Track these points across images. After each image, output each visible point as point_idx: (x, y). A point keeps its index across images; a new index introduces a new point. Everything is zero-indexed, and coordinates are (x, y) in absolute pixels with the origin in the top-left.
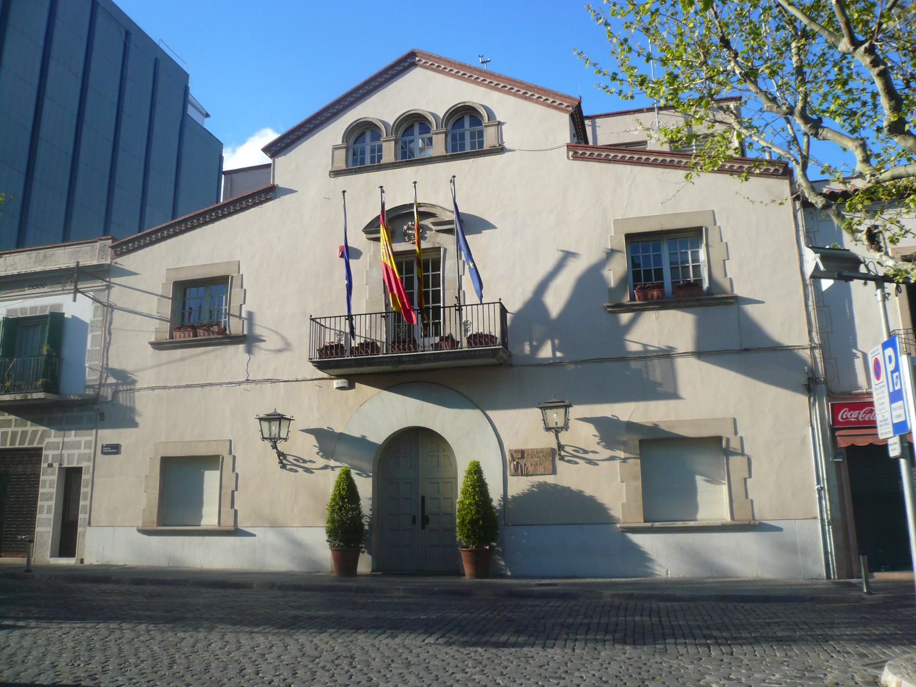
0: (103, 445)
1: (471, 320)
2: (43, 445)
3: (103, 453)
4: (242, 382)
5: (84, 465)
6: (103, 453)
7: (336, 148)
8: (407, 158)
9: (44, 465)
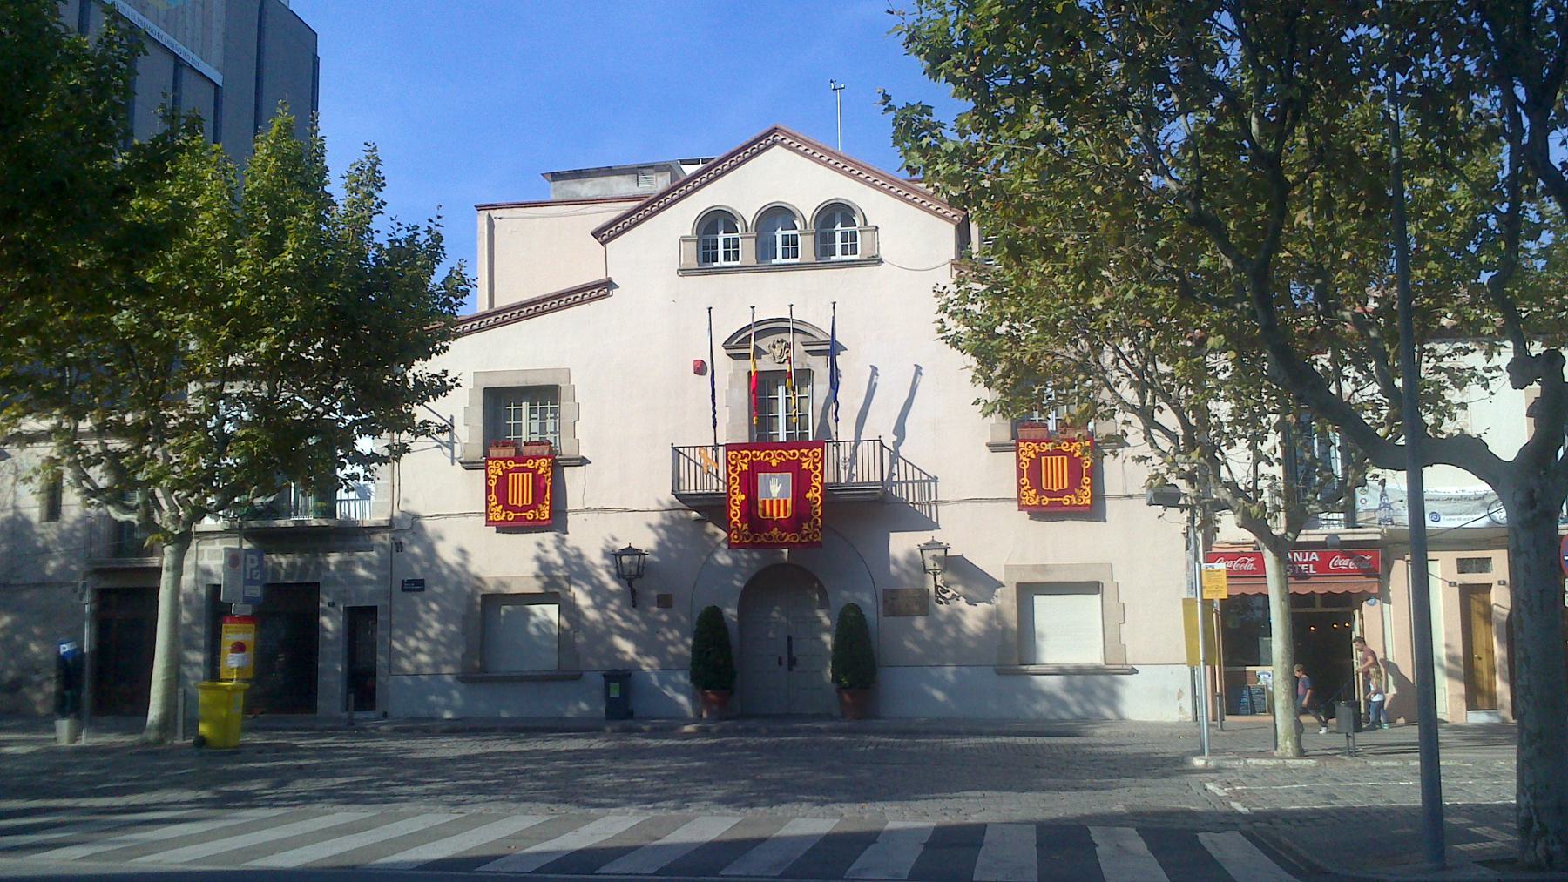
0: (403, 581)
2: (320, 580)
3: (403, 590)
4: (581, 511)
5: (379, 602)
7: (684, 240)
8: (765, 260)
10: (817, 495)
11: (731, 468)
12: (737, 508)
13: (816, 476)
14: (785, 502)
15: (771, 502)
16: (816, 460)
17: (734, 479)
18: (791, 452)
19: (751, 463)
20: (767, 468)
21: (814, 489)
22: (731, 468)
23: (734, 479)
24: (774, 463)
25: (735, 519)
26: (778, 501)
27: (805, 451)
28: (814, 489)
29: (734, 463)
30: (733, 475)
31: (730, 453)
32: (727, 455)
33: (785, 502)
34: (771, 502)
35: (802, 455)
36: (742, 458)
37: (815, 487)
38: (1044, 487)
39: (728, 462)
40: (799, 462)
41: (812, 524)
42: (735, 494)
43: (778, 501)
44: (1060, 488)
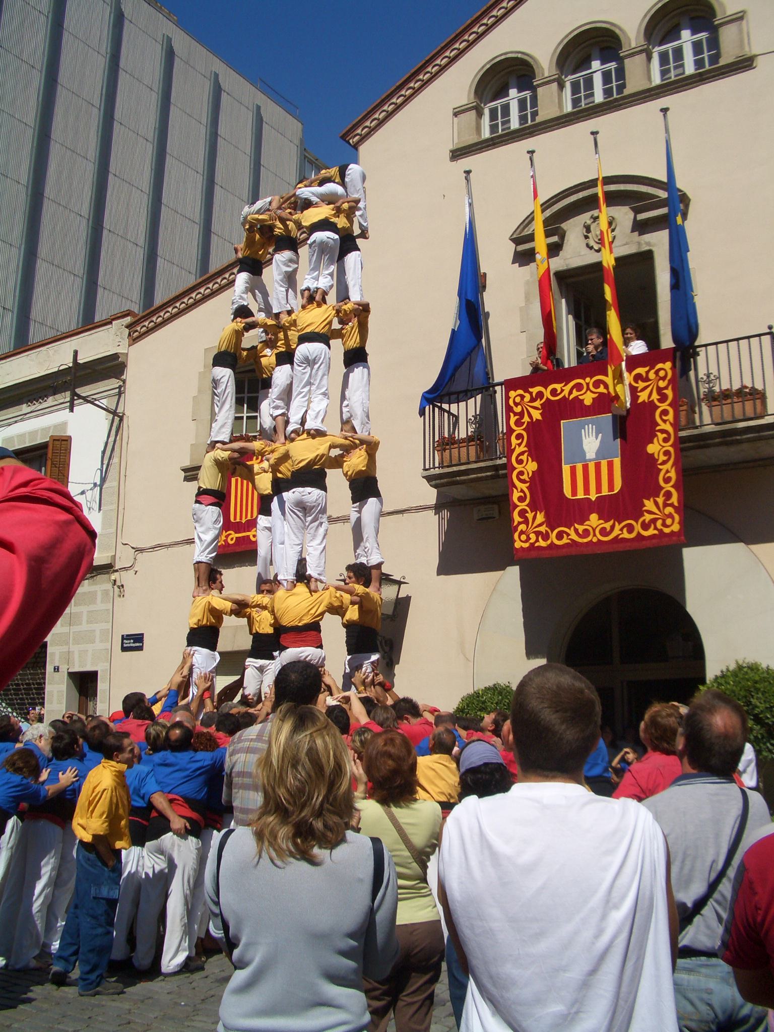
1: (716, 373)
5: (100, 667)
6: (124, 649)
9: (49, 668)
10: (519, 468)
11: (513, 419)
12: (524, 487)
13: (665, 412)
14: (610, 465)
15: (586, 468)
16: (523, 527)
17: (519, 436)
18: (565, 541)
19: (637, 513)
20: (574, 409)
21: (661, 436)
22: (513, 419)
23: (519, 436)
24: (588, 399)
25: (664, 406)
26: (598, 466)
27: (542, 543)
28: (525, 477)
29: (518, 409)
30: (519, 430)
31: (512, 394)
32: (508, 398)
33: (610, 465)
34: (586, 468)
35: (546, 537)
36: (533, 400)
37: (523, 481)
38: (232, 519)
39: (509, 409)
40: (552, 523)
41: (526, 419)
42: (667, 453)
43: (598, 466)
44: (249, 518)
